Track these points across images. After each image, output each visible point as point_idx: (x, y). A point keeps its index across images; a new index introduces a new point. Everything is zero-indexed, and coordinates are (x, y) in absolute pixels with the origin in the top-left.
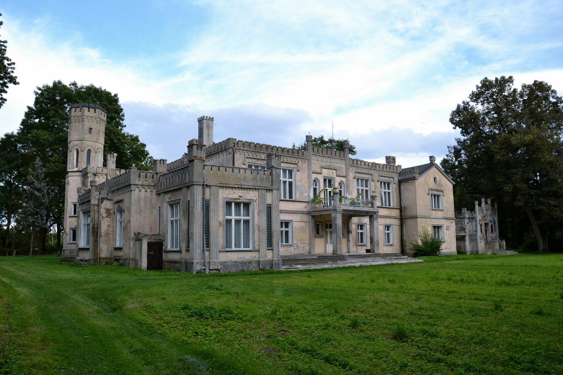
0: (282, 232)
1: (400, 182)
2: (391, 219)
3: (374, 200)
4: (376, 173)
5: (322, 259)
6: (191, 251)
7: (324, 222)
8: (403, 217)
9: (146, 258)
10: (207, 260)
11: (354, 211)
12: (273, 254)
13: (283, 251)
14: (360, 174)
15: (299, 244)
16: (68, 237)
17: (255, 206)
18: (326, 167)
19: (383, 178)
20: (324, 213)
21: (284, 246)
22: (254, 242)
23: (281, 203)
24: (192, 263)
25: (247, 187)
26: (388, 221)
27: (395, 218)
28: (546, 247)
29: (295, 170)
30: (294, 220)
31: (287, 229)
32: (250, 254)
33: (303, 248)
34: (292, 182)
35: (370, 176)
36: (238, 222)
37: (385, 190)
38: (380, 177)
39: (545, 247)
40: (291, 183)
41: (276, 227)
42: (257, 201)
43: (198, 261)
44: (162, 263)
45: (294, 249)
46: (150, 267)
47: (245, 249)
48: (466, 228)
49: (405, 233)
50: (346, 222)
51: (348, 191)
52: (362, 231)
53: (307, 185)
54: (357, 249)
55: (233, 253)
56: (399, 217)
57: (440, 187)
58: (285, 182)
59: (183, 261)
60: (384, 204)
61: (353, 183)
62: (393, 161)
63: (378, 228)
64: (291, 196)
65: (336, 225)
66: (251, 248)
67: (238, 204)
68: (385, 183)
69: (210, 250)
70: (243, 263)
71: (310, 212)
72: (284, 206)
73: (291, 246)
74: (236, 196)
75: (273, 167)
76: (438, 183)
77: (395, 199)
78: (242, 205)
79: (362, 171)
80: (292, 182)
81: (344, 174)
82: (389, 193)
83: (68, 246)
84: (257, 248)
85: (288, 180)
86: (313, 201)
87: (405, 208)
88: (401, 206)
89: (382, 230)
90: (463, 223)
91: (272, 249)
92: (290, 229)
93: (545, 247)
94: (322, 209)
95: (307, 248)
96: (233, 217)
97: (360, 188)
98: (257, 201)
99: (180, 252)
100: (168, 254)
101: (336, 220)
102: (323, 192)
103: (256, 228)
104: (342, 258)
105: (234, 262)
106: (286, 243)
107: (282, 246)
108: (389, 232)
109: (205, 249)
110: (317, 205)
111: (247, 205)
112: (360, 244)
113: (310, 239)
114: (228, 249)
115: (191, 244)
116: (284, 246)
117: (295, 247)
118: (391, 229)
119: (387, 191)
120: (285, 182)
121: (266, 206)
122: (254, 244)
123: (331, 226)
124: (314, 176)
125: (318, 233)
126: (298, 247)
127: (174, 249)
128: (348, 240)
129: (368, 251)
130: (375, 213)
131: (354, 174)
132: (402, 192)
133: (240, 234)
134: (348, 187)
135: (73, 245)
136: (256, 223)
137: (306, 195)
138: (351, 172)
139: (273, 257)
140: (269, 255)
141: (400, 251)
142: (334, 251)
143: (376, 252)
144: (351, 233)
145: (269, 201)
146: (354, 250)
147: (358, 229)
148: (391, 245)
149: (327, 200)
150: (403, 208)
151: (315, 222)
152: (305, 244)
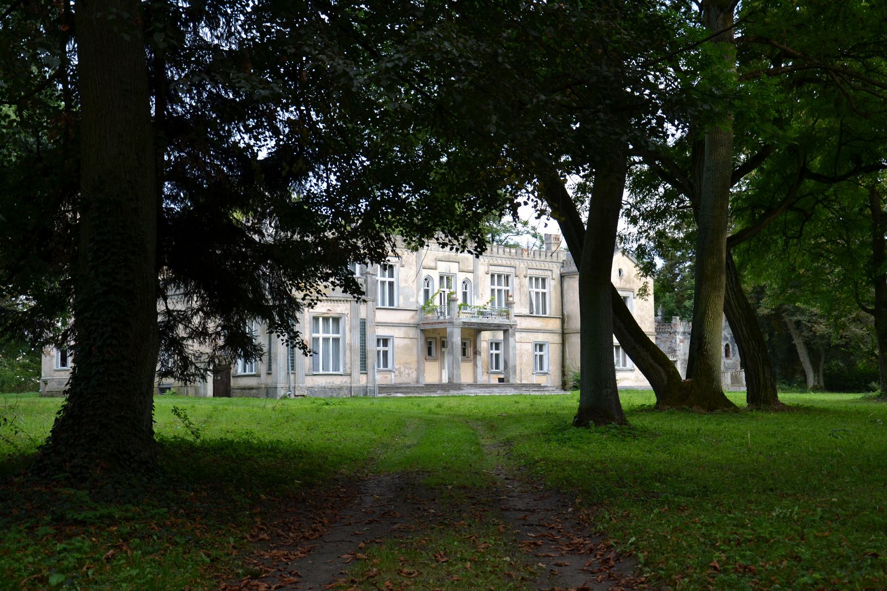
0: (379, 352)
1: (562, 277)
2: (545, 334)
3: (511, 308)
4: (522, 265)
5: (430, 387)
6: (273, 374)
7: (439, 338)
8: (565, 331)
9: (212, 385)
10: (292, 385)
11: (478, 324)
12: (367, 379)
13: (381, 379)
14: (497, 267)
15: (402, 369)
16: (54, 360)
17: (347, 322)
18: (444, 259)
19: (534, 271)
20: (437, 326)
21: (382, 371)
22: (345, 364)
23: (378, 313)
24: (276, 388)
25: (337, 299)
26: (540, 338)
27: (551, 332)
28: (819, 383)
29: (398, 265)
30: (396, 335)
31: (386, 349)
32: (340, 378)
33: (409, 374)
34: (393, 282)
35: (513, 270)
36: (326, 340)
37: (537, 290)
38: (529, 270)
39: (816, 384)
40: (391, 284)
41: (371, 345)
42: (349, 316)
43: (283, 385)
44: (230, 390)
45: (396, 376)
46: (216, 394)
47: (334, 373)
48: (677, 348)
49: (567, 355)
50: (472, 339)
51: (476, 294)
52: (497, 352)
53: (414, 286)
54: (489, 377)
55: (320, 377)
56: (560, 331)
57: (630, 283)
58: (383, 283)
59: (263, 386)
60: (535, 310)
61: (484, 281)
62: (557, 242)
63: (515, 347)
64: (391, 302)
65: (452, 343)
66: (341, 372)
67: (326, 319)
68: (537, 279)
69: (295, 374)
70: (332, 389)
71: (418, 324)
72: (381, 316)
73: (390, 371)
74: (324, 310)
75: (368, 273)
76: (624, 277)
77: (553, 302)
78: (331, 320)
79: (500, 262)
80: (393, 282)
81: (471, 268)
82: (544, 294)
83: (55, 375)
84: (348, 371)
85: (503, 288)
86: (423, 308)
87: (568, 316)
88: (563, 314)
89: (530, 351)
90: (674, 341)
91: (366, 373)
92: (389, 349)
93: (816, 384)
94: (435, 321)
95: (414, 375)
96: (321, 335)
97: (496, 287)
98: (349, 316)
99: (258, 376)
100: (239, 379)
101: (452, 336)
102: (438, 295)
103: (348, 347)
104: (459, 387)
105: (322, 387)
106: (384, 367)
107: (379, 371)
108: (541, 353)
109: (291, 372)
110: (429, 315)
111: (336, 320)
112: (494, 370)
113: (418, 362)
114: (315, 373)
115: (273, 366)
116: (382, 371)
117: (397, 373)
118: (545, 348)
119: (541, 290)
120: (383, 283)
121: (359, 321)
122: (344, 367)
123: (443, 345)
124: (425, 273)
125: (430, 353)
126: (400, 373)
127: (247, 373)
128: (475, 365)
129: (501, 380)
130: (511, 326)
131: (486, 267)
132: (565, 292)
133: (328, 355)
134: (476, 287)
135: (63, 373)
136: (348, 341)
137: (413, 300)
138: (482, 264)
139: (367, 383)
140: (363, 380)
141: (561, 383)
142: (449, 379)
143: (511, 381)
144: (480, 355)
145: (363, 315)
146: (482, 379)
147: (492, 349)
148: (545, 374)
149: (445, 308)
150: (566, 317)
151: (426, 339)
152: (411, 369)
